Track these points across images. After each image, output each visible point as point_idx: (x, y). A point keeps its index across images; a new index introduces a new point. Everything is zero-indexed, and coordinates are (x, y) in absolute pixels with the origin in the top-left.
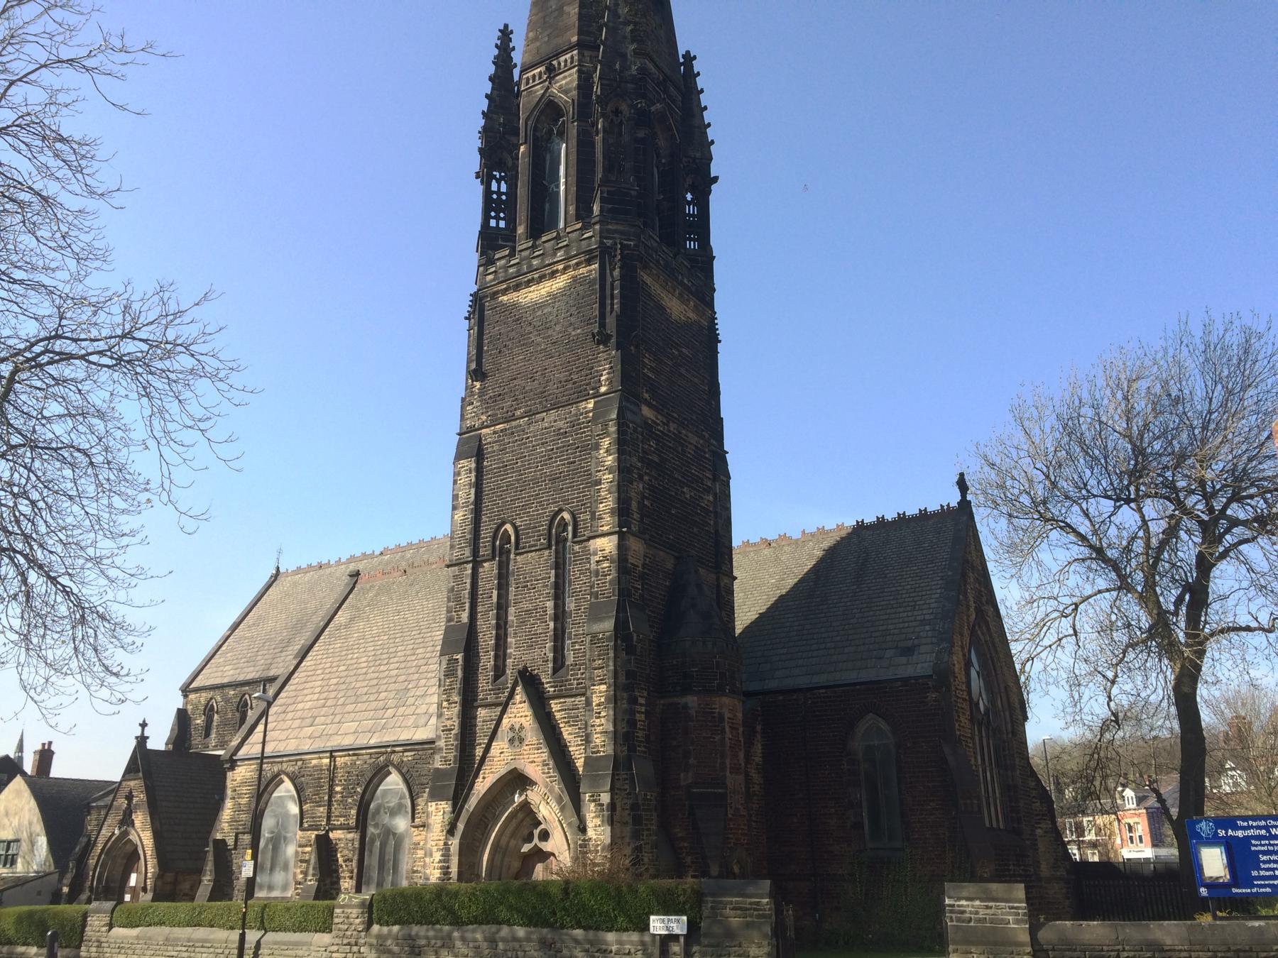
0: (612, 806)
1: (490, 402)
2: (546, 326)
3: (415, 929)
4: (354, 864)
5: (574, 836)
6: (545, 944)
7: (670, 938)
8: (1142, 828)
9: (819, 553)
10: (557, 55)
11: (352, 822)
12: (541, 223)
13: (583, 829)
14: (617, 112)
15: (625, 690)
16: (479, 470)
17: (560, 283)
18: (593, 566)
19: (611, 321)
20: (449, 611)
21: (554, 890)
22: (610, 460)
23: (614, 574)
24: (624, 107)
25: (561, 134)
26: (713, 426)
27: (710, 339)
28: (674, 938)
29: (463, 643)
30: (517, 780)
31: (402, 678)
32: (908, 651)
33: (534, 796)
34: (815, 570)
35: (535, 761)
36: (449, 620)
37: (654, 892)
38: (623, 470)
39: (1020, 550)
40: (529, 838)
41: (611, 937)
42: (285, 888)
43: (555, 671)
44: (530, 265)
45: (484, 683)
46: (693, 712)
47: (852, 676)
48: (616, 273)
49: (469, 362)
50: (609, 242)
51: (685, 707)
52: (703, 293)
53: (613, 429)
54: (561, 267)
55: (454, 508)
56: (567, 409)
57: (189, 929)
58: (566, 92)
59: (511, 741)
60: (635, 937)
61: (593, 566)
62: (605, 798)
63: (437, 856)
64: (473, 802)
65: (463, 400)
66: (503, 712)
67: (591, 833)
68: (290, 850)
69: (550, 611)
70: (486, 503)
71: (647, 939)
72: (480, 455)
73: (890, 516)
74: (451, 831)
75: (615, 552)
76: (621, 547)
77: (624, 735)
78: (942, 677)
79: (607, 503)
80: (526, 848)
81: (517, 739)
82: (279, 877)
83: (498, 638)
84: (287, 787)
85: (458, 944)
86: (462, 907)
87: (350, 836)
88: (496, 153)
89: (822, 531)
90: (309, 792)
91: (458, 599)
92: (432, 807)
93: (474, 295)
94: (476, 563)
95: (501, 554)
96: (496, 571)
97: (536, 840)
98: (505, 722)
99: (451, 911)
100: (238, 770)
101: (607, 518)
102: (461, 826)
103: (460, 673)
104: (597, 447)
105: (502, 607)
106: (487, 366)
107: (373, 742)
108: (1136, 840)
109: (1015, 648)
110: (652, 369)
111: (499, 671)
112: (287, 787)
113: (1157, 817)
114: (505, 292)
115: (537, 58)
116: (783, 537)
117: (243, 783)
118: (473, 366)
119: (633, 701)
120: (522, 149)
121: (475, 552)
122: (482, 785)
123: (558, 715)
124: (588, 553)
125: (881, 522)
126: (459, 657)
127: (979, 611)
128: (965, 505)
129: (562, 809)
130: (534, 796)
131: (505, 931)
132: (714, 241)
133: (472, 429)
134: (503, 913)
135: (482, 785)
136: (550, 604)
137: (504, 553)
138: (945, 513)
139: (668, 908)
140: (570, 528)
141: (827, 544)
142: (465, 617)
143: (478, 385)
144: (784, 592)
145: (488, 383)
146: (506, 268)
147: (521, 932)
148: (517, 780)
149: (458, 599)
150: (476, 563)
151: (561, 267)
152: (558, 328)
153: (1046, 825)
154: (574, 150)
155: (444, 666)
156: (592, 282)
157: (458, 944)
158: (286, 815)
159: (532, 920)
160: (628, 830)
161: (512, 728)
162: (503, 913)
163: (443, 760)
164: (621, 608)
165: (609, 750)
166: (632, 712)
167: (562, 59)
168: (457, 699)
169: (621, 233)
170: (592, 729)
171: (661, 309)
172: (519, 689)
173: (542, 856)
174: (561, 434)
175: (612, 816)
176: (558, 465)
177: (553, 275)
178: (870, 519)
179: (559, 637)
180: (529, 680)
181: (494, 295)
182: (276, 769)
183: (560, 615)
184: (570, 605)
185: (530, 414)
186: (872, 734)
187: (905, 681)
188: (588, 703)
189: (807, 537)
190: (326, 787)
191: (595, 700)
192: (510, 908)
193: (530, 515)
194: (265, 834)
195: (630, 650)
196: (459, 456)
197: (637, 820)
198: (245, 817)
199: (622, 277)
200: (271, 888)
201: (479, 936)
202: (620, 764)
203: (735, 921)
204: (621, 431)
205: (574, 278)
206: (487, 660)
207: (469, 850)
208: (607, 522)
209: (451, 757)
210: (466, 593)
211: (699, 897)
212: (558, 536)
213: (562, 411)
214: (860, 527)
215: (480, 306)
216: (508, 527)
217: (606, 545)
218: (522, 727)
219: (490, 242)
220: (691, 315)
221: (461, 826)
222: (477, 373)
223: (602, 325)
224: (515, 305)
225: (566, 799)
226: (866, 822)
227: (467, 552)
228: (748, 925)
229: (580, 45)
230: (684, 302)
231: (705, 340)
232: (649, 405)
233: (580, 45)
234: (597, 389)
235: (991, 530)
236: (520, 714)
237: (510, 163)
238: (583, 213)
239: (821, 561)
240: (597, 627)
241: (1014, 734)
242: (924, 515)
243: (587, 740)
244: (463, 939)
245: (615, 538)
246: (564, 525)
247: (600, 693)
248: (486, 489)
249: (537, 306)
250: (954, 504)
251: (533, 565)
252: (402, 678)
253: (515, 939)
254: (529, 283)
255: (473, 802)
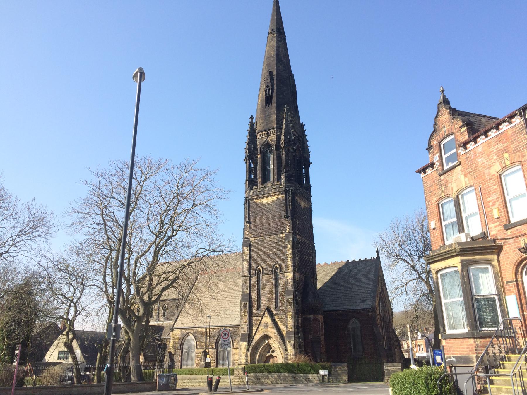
0: (294, 344)
1: (252, 231)
2: (269, 211)
3: (258, 374)
4: (215, 359)
5: (282, 353)
6: (293, 377)
7: (323, 376)
8: (423, 346)
9: (336, 269)
10: (270, 130)
11: (214, 347)
12: (265, 179)
13: (286, 350)
14: (288, 150)
15: (296, 313)
16: (250, 250)
17: (273, 199)
18: (286, 281)
19: (289, 212)
20: (243, 289)
21: (295, 365)
22: (290, 252)
23: (292, 283)
24: (290, 149)
25: (270, 152)
26: (311, 236)
27: (310, 210)
28: (326, 375)
29: (248, 299)
30: (266, 337)
31: (223, 306)
32: (364, 301)
33: (271, 341)
34: (336, 275)
35: (272, 332)
36: (243, 292)
37: (320, 365)
38: (294, 254)
39: (392, 267)
40: (269, 352)
41: (310, 375)
42: (192, 365)
43: (276, 308)
44: (264, 193)
45: (254, 310)
46: (312, 319)
47: (348, 308)
48: (290, 198)
49: (245, 218)
50: (288, 189)
51: (310, 318)
52: (308, 199)
53: (291, 243)
54: (273, 194)
55: (243, 261)
56: (277, 236)
57: (189, 376)
58: (273, 141)
59: (265, 327)
60: (316, 375)
61: (286, 281)
62: (293, 342)
63: (244, 357)
64: (254, 343)
65: (244, 229)
66: (262, 319)
67: (289, 351)
68: (193, 355)
69: (274, 292)
70: (253, 260)
71: (319, 375)
72: (250, 246)
73: (357, 260)
74: (248, 350)
75: (293, 277)
76: (294, 276)
77: (296, 326)
78: (373, 309)
79: (290, 263)
80: (268, 355)
81: (266, 326)
82: (190, 362)
83: (258, 298)
84: (191, 337)
85: (270, 377)
86: (271, 369)
87: (213, 351)
88: (251, 156)
89: (337, 263)
90: (199, 338)
91: (246, 287)
92: (241, 343)
93: (246, 198)
94: (251, 277)
95: (258, 274)
96: (256, 279)
97: (271, 353)
98: (262, 321)
99: (268, 370)
100: (174, 331)
101: (290, 268)
102: (251, 349)
103: (248, 307)
104: (286, 248)
105: (259, 289)
106: (251, 220)
107: (219, 325)
108: (421, 350)
109: (389, 295)
110: (299, 224)
111: (259, 307)
112: (191, 337)
113: (428, 342)
114: (256, 199)
115: (263, 129)
116: (325, 264)
117: (176, 335)
118: (247, 220)
119: (298, 317)
120: (259, 156)
121: (250, 274)
122: (256, 338)
123: (277, 320)
124: (284, 277)
125: (354, 261)
126: (247, 303)
127: (382, 288)
128: (378, 258)
129: (280, 345)
130: (271, 341)
131: (282, 374)
132: (311, 182)
133: (247, 238)
134: (282, 370)
135: (256, 338)
136: (273, 290)
137: (259, 274)
138: (372, 260)
139: (324, 368)
140: (279, 269)
141: (339, 267)
142: (248, 292)
143: (249, 225)
144: (327, 281)
145: (252, 225)
146: (256, 192)
147: (287, 375)
148: (266, 337)
149: (246, 287)
150: (251, 277)
151: (273, 194)
152: (273, 212)
153: (398, 348)
154: (275, 157)
155: (243, 305)
156: (283, 200)
157: (270, 377)
158: (191, 345)
159: (290, 372)
160: (298, 350)
161: (265, 323)
162: (282, 370)
163: (244, 330)
164: (295, 292)
165: (293, 330)
166: (298, 320)
167: (271, 131)
168: (247, 314)
169: (291, 186)
170: (288, 323)
171: (300, 205)
172: (266, 313)
173: (272, 357)
174: (274, 242)
175: (295, 347)
176: (274, 251)
177: (271, 196)
178: (351, 260)
179: (276, 299)
180: (269, 310)
181: (253, 199)
182: (187, 331)
183: (276, 293)
184: (279, 290)
185: (265, 236)
186: (354, 324)
187: (363, 309)
188: (286, 317)
189: (332, 264)
190: (205, 337)
191: (288, 317)
192: (284, 369)
193: (267, 264)
194: (184, 350)
195: (297, 303)
196: (243, 246)
197: (300, 348)
198: (178, 346)
199: (292, 199)
200: (187, 365)
201: (276, 376)
202: (296, 333)
203: (340, 372)
204: (293, 244)
205: (278, 198)
206: (255, 304)
207: (253, 355)
208: (290, 269)
209: (246, 330)
210: (248, 285)
211: (331, 367)
212: (275, 271)
213: (275, 236)
214: (348, 262)
215: (248, 202)
216: (260, 267)
217: (290, 275)
218: (268, 323)
219: (251, 183)
220: (306, 205)
221: (251, 349)
222: (249, 222)
223: (287, 213)
224: (259, 203)
225: (281, 342)
226: (322, 338)
227: (248, 273)
228: (343, 373)
229: (277, 128)
230: (304, 202)
231: (309, 210)
232: (298, 235)
233: (277, 128)
234: (285, 231)
235: (384, 261)
236: (267, 319)
237: (255, 158)
238: (279, 179)
239: (337, 272)
240: (288, 297)
241: (390, 322)
242: (366, 260)
243: (287, 327)
244: (272, 376)
245: (292, 273)
246: (276, 268)
247: (290, 315)
248: (252, 256)
249: (266, 205)
250: (375, 257)
251: (268, 278)
252: (223, 306)
253: (285, 376)
254: (263, 197)
255: (254, 343)
